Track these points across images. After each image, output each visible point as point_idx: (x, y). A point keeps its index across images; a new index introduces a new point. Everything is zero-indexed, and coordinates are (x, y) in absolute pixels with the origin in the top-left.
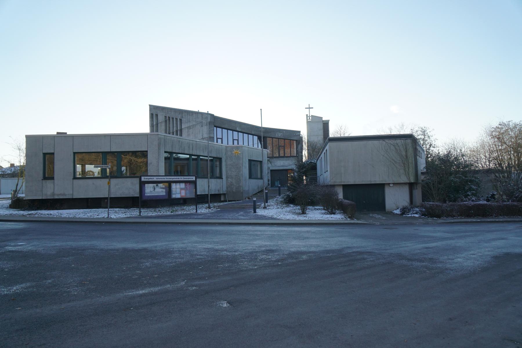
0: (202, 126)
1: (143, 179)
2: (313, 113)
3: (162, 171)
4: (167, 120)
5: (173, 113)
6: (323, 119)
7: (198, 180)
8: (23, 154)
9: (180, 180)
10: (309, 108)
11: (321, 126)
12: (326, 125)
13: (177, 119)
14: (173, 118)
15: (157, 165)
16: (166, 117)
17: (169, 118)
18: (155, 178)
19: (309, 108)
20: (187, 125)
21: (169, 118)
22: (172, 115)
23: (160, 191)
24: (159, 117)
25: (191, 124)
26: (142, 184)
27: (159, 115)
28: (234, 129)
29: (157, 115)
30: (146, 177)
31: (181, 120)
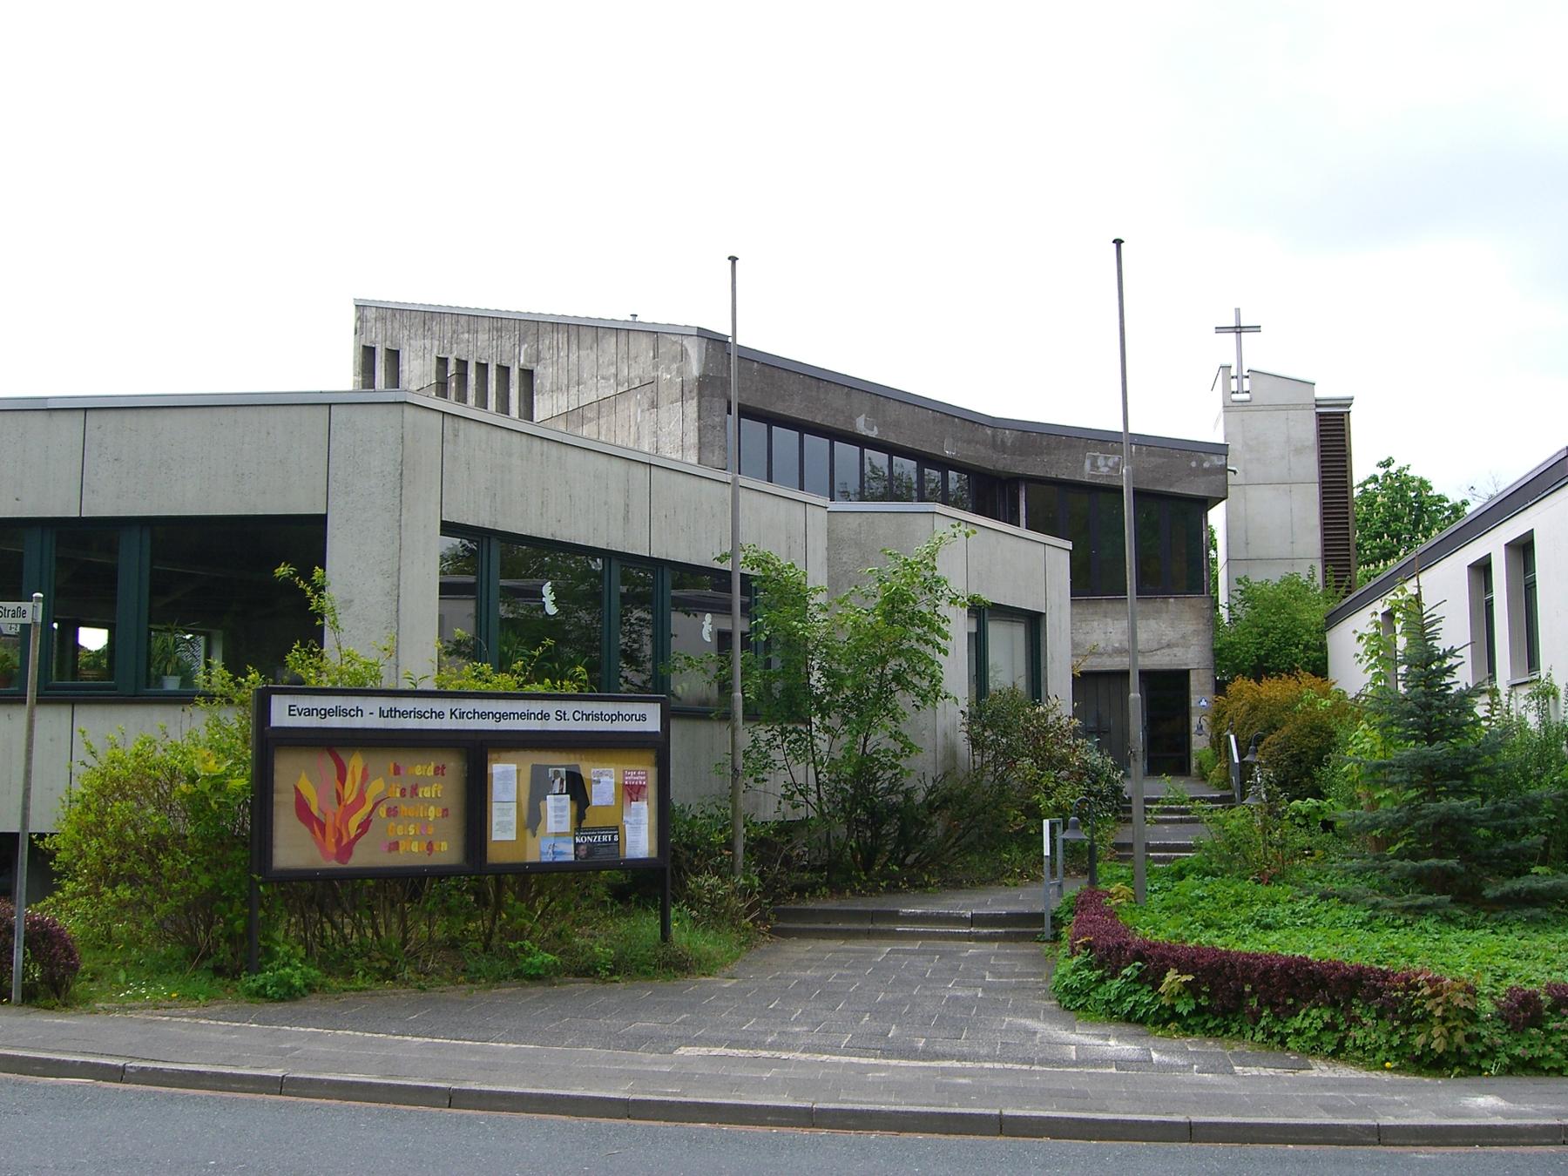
0: (654, 405)
1: (283, 713)
2: (1259, 354)
3: (420, 660)
4: (452, 377)
5: (483, 337)
6: (1321, 392)
7: (676, 728)
8: (536, 859)
9: (553, 725)
10: (1238, 329)
11: (1307, 431)
12: (1333, 428)
13: (504, 371)
14: (482, 368)
15: (384, 611)
16: (442, 362)
17: (462, 365)
18: (372, 705)
19: (1238, 329)
20: (563, 403)
21: (462, 365)
22: (479, 348)
23: (409, 823)
24: (405, 366)
25: (589, 396)
26: (269, 742)
27: (404, 356)
28: (839, 423)
29: (394, 356)
30: (304, 702)
31: (527, 375)
